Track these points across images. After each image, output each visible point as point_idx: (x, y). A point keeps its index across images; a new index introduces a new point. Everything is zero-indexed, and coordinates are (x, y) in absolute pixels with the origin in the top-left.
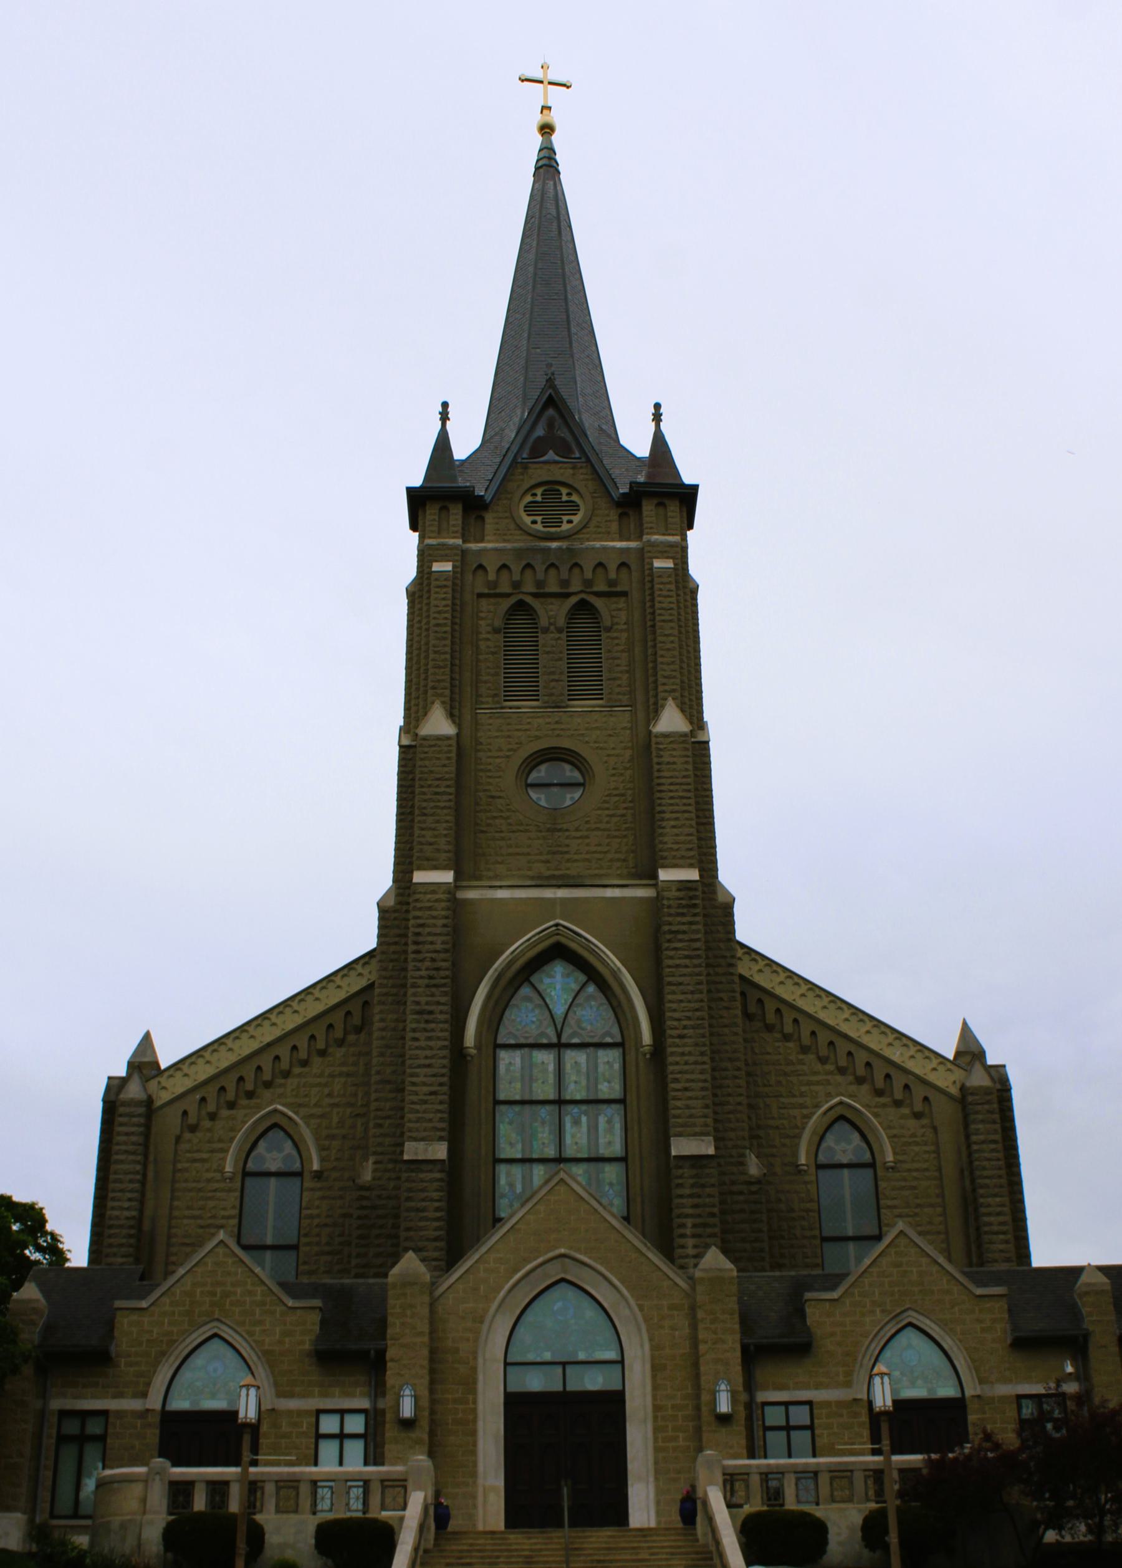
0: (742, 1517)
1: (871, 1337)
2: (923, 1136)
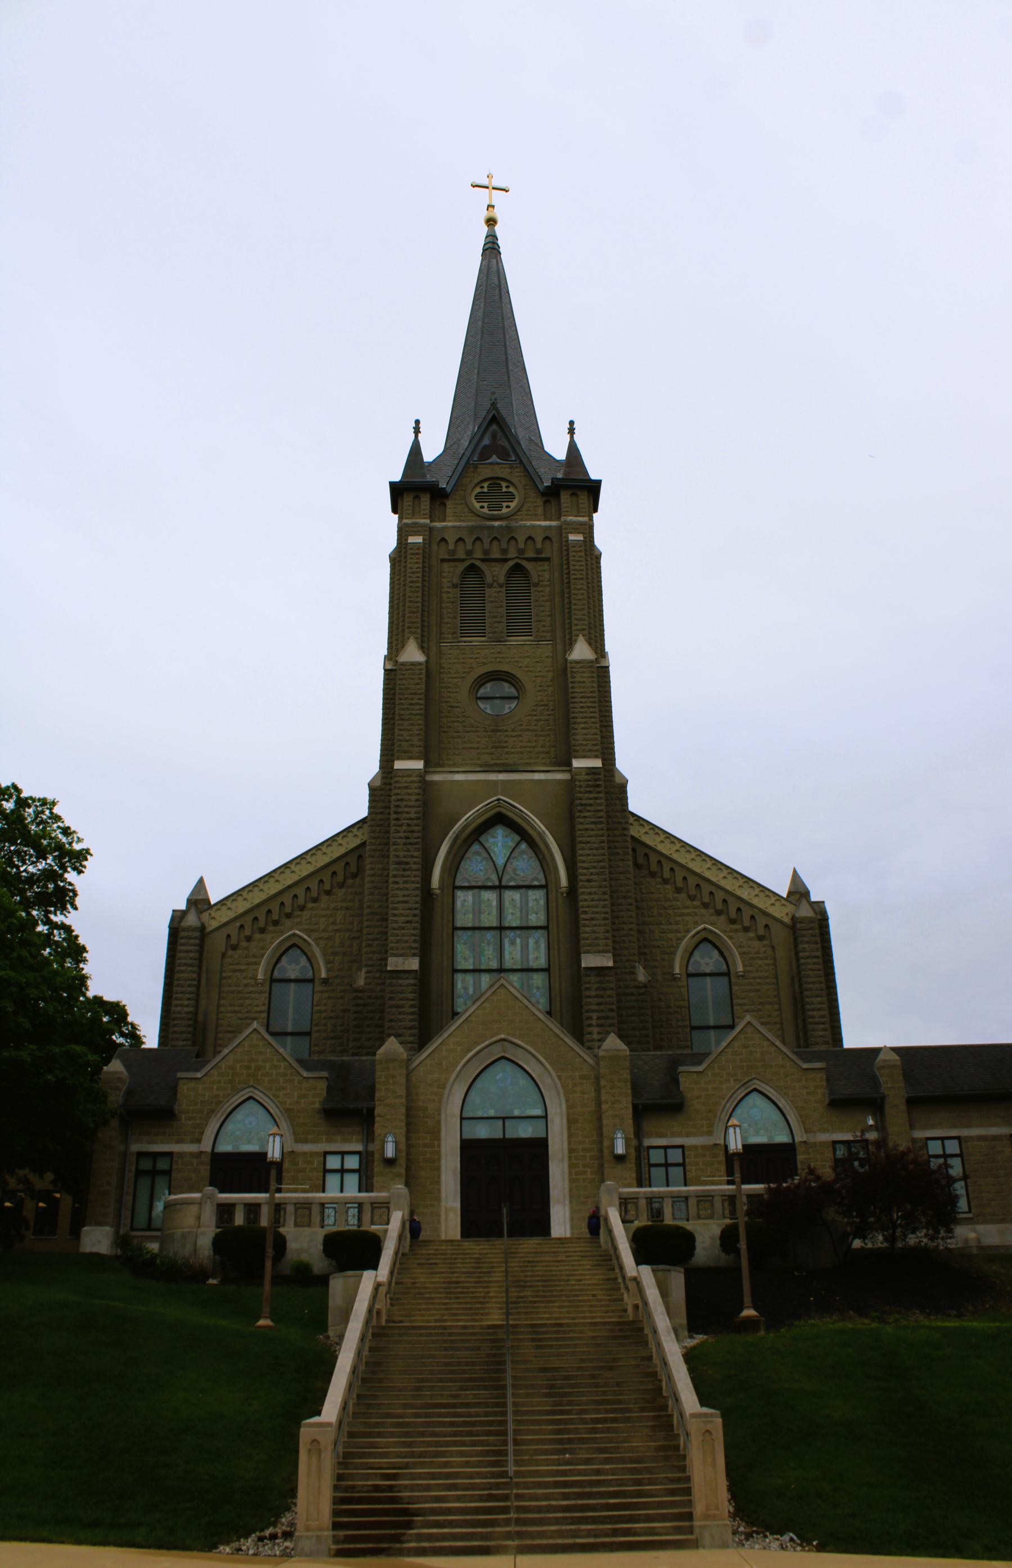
0: (634, 1229)
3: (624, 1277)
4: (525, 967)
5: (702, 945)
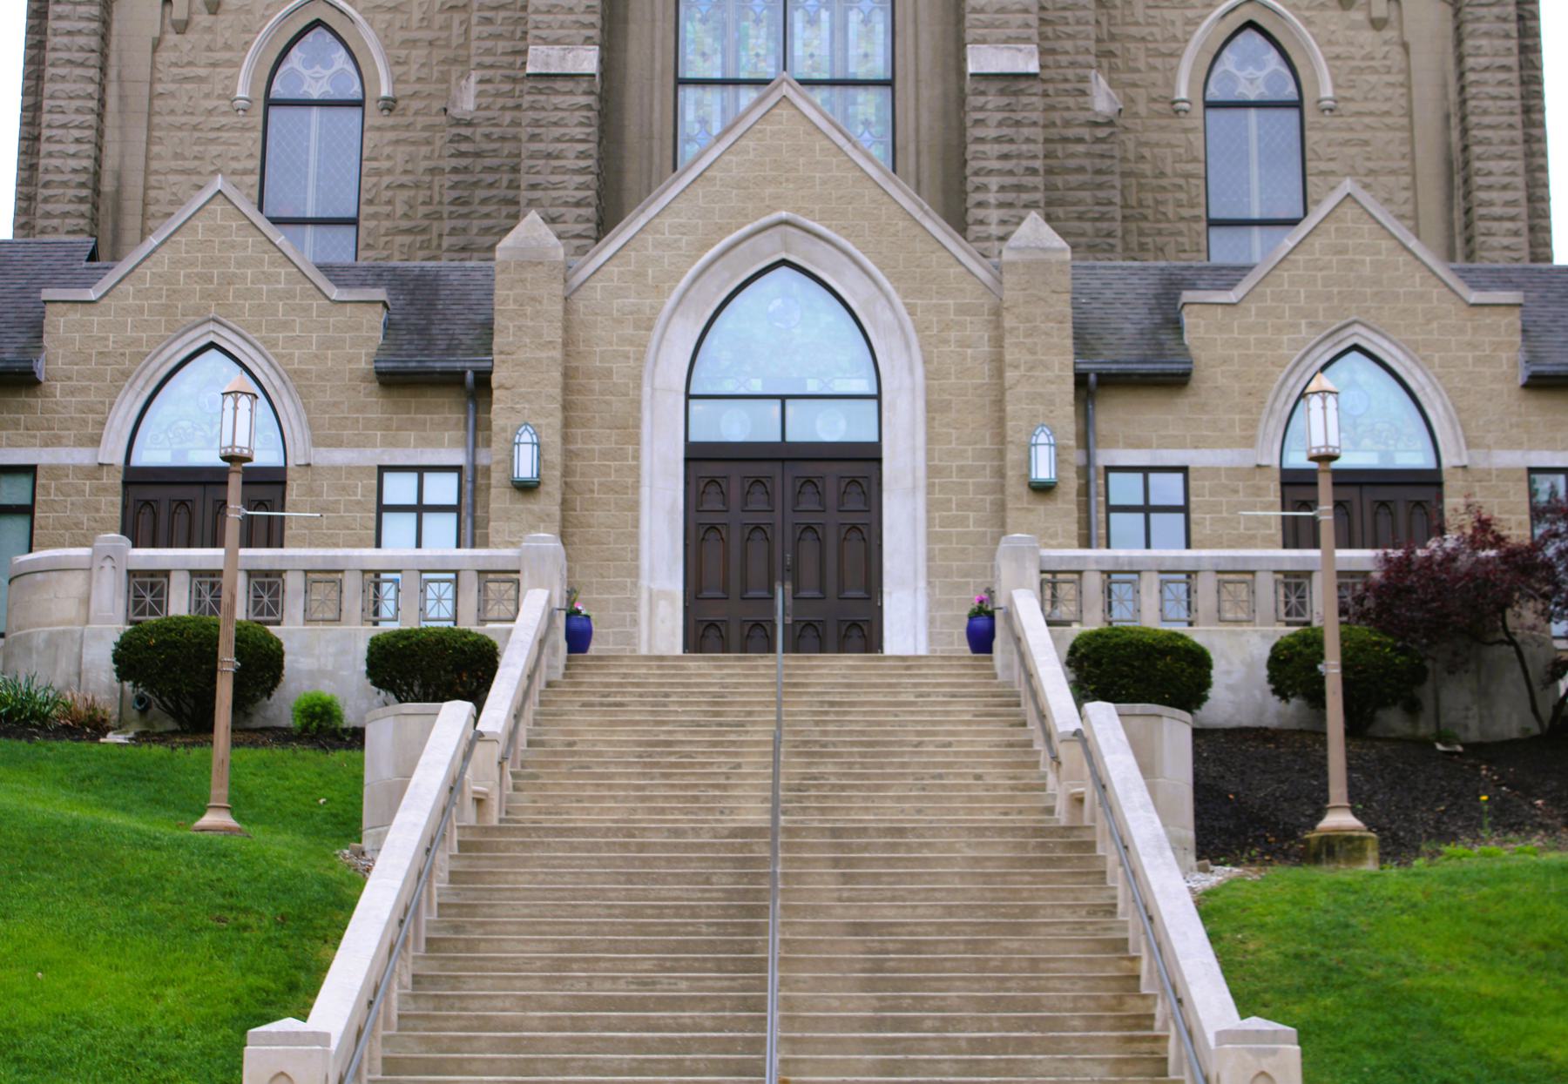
0: (1070, 641)
1: (1289, 367)
2: (1385, 58)
3: (1048, 736)
4: (839, 76)
5: (1240, 39)
